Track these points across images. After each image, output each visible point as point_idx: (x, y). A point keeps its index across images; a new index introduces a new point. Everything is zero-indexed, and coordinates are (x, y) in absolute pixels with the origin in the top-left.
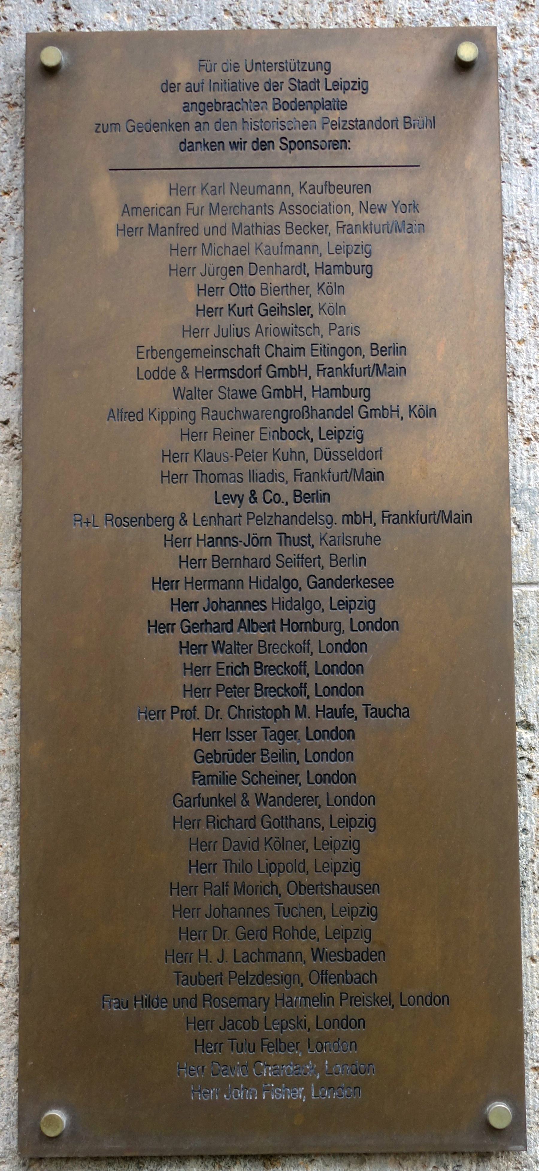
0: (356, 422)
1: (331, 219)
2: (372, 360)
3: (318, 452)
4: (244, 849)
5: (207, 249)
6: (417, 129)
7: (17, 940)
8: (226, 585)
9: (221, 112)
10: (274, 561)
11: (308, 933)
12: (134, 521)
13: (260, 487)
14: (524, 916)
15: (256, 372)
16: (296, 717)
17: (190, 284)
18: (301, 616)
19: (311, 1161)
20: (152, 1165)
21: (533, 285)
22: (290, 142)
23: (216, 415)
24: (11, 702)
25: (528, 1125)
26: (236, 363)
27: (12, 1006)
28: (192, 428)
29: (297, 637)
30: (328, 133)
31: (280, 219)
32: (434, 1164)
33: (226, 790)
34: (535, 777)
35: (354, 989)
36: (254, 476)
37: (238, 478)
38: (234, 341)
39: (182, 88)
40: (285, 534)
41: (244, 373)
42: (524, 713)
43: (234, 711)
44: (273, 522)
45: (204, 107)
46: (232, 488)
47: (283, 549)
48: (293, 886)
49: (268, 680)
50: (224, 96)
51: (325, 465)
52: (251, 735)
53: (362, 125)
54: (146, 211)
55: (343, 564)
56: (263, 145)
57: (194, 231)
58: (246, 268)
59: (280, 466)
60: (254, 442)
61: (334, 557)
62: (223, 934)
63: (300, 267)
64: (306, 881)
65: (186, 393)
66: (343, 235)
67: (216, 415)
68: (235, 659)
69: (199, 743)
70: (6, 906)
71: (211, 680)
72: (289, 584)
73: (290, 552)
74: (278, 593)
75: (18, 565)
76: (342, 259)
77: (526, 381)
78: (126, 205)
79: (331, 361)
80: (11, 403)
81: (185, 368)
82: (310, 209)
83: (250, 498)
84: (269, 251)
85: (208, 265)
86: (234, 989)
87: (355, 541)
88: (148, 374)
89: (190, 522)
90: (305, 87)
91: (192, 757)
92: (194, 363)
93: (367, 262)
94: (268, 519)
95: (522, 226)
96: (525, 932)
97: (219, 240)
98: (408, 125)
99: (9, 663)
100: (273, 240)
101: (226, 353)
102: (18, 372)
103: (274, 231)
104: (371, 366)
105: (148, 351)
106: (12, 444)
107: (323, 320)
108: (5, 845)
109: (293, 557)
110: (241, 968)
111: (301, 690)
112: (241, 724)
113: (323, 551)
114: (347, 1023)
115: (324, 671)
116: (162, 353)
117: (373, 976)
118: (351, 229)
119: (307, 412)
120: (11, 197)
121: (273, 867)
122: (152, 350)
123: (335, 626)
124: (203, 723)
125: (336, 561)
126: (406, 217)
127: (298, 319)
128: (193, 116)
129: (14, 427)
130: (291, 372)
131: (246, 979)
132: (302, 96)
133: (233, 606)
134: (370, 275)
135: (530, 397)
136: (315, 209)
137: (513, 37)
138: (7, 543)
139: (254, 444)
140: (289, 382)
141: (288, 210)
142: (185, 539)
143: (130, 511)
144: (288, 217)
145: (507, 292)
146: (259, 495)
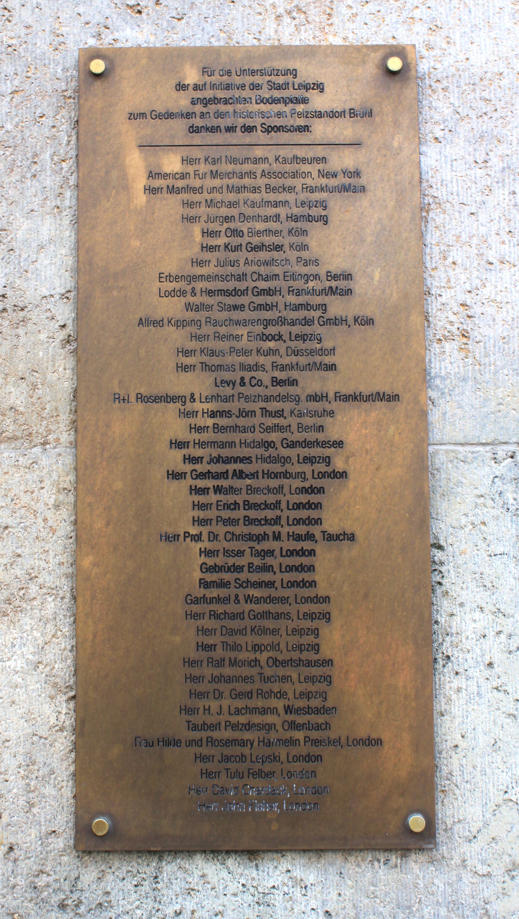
0: (317, 329)
1: (298, 183)
2: (328, 284)
3: (289, 349)
4: (236, 634)
5: (210, 203)
6: (359, 118)
7: (74, 697)
8: (223, 445)
9: (219, 105)
10: (257, 429)
11: (282, 695)
12: (157, 399)
13: (246, 375)
14: (436, 683)
15: (244, 292)
16: (273, 540)
17: (197, 230)
18: (277, 468)
19: (283, 856)
20: (169, 858)
21: (442, 228)
22: (268, 127)
23: (216, 323)
24: (68, 527)
25: (437, 831)
26: (231, 285)
27: (70, 744)
28: (199, 332)
29: (274, 483)
30: (295, 121)
31: (261, 182)
32: (370, 859)
33: (222, 592)
34: (444, 583)
35: (314, 735)
36: (243, 367)
37: (230, 368)
38: (230, 270)
39: (191, 88)
40: (265, 408)
41: (235, 292)
42: (436, 538)
43: (229, 536)
44: (256, 400)
45: (206, 102)
46: (227, 376)
47: (263, 420)
48: (271, 661)
49: (253, 514)
50: (221, 94)
51: (294, 359)
52: (240, 553)
53: (319, 115)
54: (166, 176)
55: (307, 431)
56: (249, 129)
57: (199, 190)
58: (237, 217)
59: (262, 360)
60: (243, 342)
61: (300, 426)
62: (221, 695)
63: (276, 216)
64: (280, 658)
65: (194, 307)
66: (306, 194)
67: (216, 323)
68: (231, 498)
69: (203, 559)
70: (65, 673)
71: (212, 514)
72: (269, 445)
73: (270, 421)
74: (260, 451)
75: (73, 429)
76: (305, 211)
77: (438, 298)
78: (151, 172)
79: (299, 284)
80: (67, 312)
81: (193, 289)
82: (283, 175)
83: (240, 383)
84: (253, 205)
85: (210, 215)
86: (227, 734)
87: (315, 414)
88: (167, 293)
89: (198, 400)
90: (279, 87)
91: (199, 569)
92: (199, 285)
93: (323, 213)
94: (253, 398)
95: (434, 187)
96: (436, 695)
97: (218, 197)
98: (352, 115)
99: (67, 500)
100: (256, 197)
101: (224, 278)
102: (72, 290)
103: (257, 190)
104: (327, 288)
105: (167, 276)
106: (68, 342)
107: (292, 255)
108: (64, 630)
109: (271, 426)
110: (234, 719)
111: (277, 521)
112: (235, 545)
113: (293, 421)
114: (308, 758)
115: (293, 506)
116: (177, 278)
117: (328, 725)
118: (312, 190)
119: (281, 321)
120: (67, 164)
121: (257, 648)
122: (170, 276)
123: (302, 475)
124: (205, 544)
125: (301, 427)
126: (353, 181)
127: (275, 255)
128: (199, 108)
129: (70, 329)
130: (269, 292)
131: (235, 727)
132: (277, 94)
133: (228, 460)
134: (326, 223)
135: (441, 310)
136: (286, 175)
137: (427, 50)
138: (65, 413)
139: (244, 343)
140: (269, 299)
141: (267, 176)
142: (193, 412)
143: (155, 392)
144: (266, 181)
145: (424, 233)
146: (247, 381)
